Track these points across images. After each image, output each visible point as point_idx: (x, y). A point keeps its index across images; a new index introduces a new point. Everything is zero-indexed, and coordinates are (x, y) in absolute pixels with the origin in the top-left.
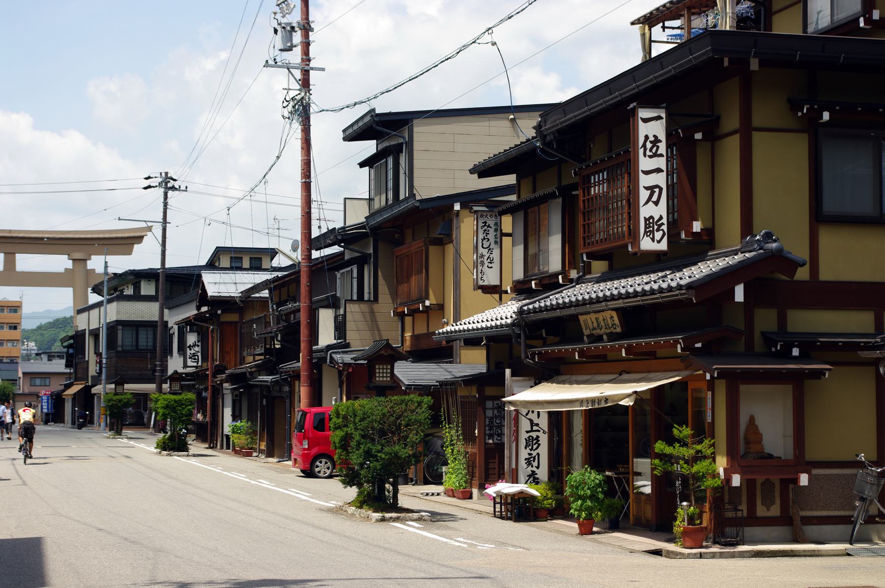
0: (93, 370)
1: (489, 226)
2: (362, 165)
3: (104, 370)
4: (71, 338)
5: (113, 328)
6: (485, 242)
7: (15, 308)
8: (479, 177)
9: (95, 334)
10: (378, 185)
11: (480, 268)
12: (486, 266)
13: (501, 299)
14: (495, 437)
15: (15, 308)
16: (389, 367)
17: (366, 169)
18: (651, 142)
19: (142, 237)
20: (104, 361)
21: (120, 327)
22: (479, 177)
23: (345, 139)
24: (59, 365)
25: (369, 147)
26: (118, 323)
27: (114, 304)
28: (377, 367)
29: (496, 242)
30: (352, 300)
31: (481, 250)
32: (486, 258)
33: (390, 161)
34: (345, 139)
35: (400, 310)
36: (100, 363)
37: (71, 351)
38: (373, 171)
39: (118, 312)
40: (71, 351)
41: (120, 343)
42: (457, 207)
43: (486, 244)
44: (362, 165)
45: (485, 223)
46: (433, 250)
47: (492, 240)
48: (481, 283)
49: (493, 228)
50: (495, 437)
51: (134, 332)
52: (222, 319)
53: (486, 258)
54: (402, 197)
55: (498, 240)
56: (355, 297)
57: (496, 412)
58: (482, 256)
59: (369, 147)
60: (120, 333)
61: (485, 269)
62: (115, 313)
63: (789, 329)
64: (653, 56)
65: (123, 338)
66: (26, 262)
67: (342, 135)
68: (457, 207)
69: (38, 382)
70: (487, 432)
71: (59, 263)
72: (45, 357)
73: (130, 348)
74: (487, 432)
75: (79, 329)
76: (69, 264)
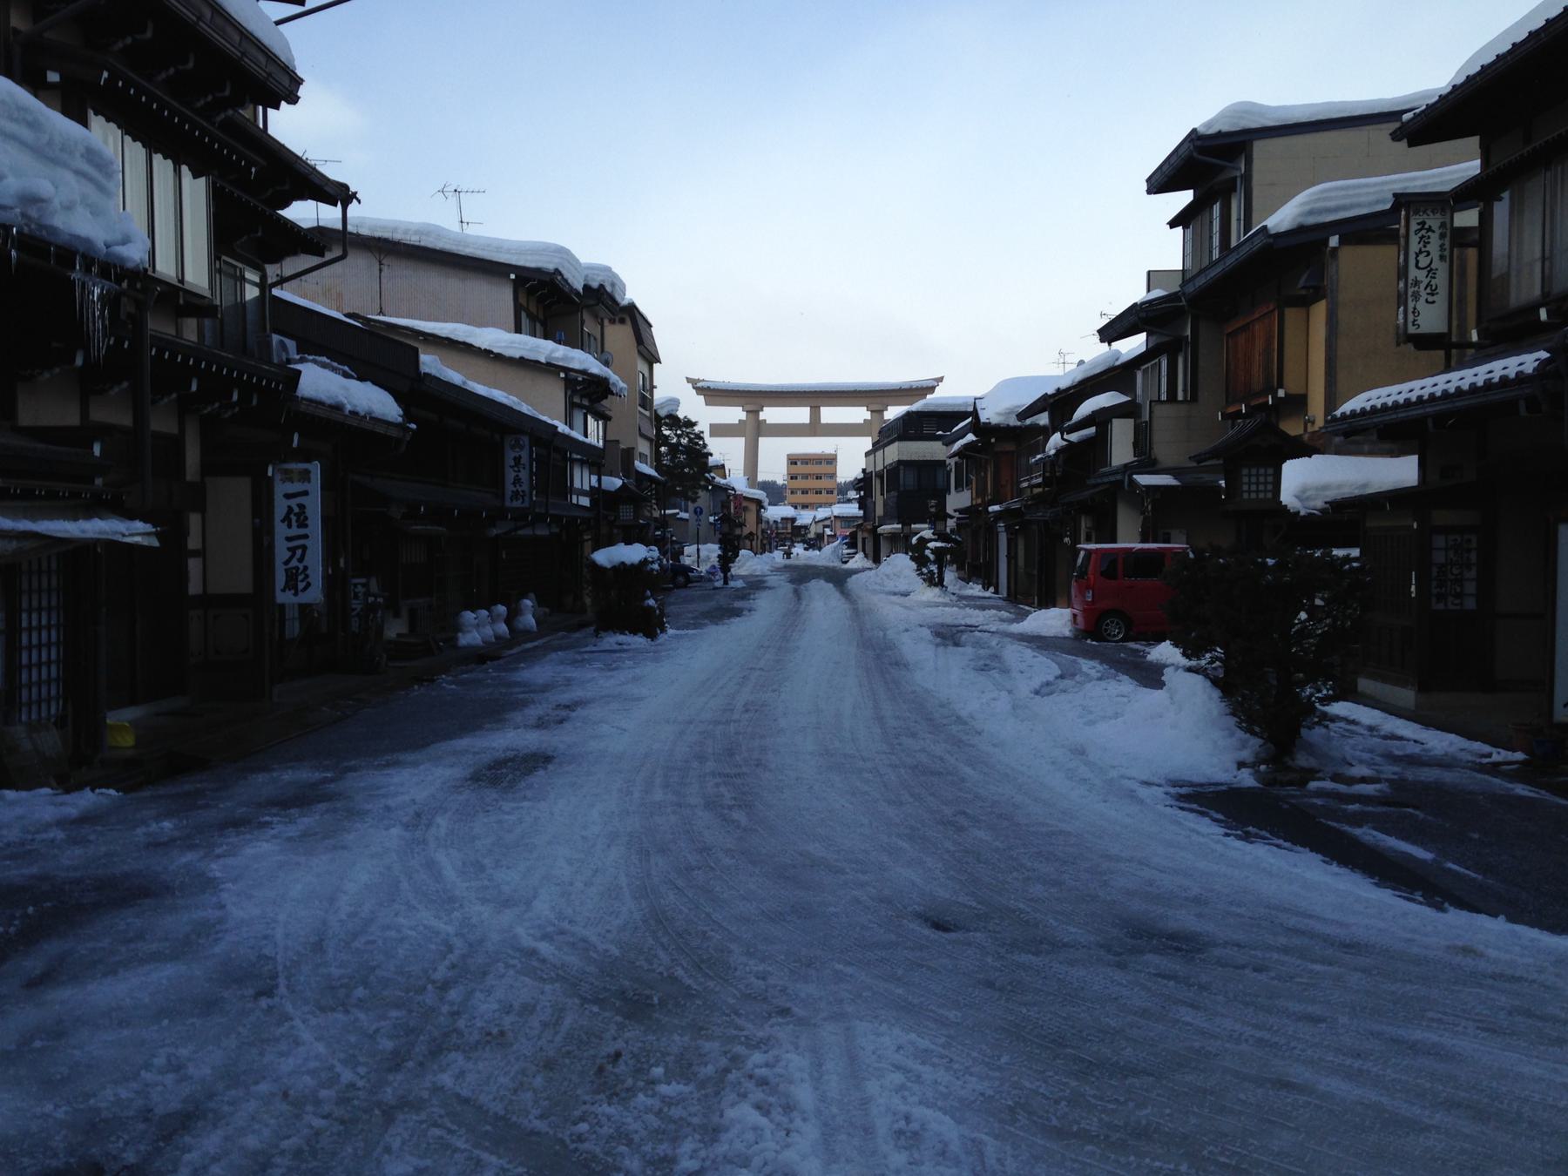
1: (1430, 229)
2: (1173, 224)
6: (1421, 257)
7: (831, 460)
8: (1410, 145)
10: (1194, 248)
11: (1411, 305)
12: (1422, 300)
13: (1448, 358)
14: (1450, 599)
15: (831, 460)
16: (1270, 471)
17: (1180, 229)
22: (1410, 145)
23: (1149, 192)
25: (1182, 199)
26: (900, 462)
28: (1245, 471)
29: (1442, 258)
30: (1159, 401)
31: (1413, 273)
32: (1422, 286)
33: (1217, 208)
34: (1149, 192)
35: (1231, 410)
38: (1189, 231)
42: (1334, 241)
43: (1424, 261)
44: (1173, 224)
45: (1423, 223)
46: (1292, 315)
47: (1435, 254)
48: (1412, 330)
49: (1438, 232)
50: (1450, 599)
52: (998, 449)
53: (1422, 286)
54: (1234, 243)
55: (1447, 253)
56: (1164, 397)
57: (1451, 554)
58: (1417, 283)
59: (1182, 199)
61: (1421, 305)
64: (1323, 302)
65: (908, 479)
66: (829, 415)
67: (1145, 187)
68: (1334, 241)
70: (1435, 591)
71: (858, 414)
74: (1435, 591)
76: (868, 415)
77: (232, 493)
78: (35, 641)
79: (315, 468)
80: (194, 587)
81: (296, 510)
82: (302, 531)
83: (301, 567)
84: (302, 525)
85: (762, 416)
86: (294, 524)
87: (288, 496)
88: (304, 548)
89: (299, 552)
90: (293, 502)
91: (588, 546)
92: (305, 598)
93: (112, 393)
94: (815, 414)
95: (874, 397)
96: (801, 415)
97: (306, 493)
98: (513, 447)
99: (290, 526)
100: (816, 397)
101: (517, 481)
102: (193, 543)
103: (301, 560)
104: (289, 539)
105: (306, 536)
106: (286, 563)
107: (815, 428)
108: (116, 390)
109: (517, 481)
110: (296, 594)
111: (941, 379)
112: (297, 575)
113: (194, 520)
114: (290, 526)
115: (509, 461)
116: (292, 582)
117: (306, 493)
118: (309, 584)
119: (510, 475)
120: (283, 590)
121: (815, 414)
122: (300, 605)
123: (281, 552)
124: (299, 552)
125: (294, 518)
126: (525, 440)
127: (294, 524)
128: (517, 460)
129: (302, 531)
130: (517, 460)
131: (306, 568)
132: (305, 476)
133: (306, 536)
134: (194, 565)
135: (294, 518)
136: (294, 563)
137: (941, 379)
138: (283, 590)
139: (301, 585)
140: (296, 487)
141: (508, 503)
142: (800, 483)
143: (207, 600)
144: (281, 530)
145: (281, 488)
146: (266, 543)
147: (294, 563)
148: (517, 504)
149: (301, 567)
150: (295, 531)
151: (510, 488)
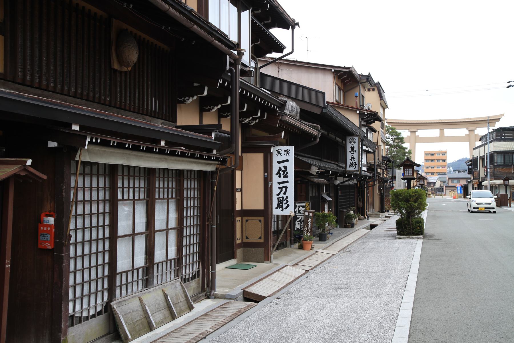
0: (482, 174)
3: (489, 174)
4: (471, 161)
5: (492, 156)
9: (483, 159)
18: (282, 171)
19: (499, 119)
20: (489, 170)
21: (496, 154)
24: (465, 175)
27: (493, 143)
36: (487, 171)
37: (470, 167)
39: (494, 147)
40: (470, 167)
41: (495, 161)
51: (503, 156)
60: (495, 157)
62: (493, 148)
63: (178, 105)
66: (449, 132)
69: (455, 181)
71: (463, 132)
72: (457, 172)
73: (500, 164)
75: (475, 157)
76: (467, 132)
77: (254, 161)
78: (87, 238)
79: (292, 148)
80: (238, 207)
81: (283, 169)
82: (285, 179)
83: (285, 197)
84: (286, 176)
85: (417, 134)
86: (282, 176)
87: (279, 162)
88: (286, 187)
89: (284, 189)
90: (282, 165)
91: (43, 214)
92: (286, 212)
93: (188, 102)
94: (442, 133)
95: (471, 124)
96: (435, 132)
97: (287, 161)
98: (350, 142)
99: (280, 177)
100: (442, 125)
101: (352, 158)
102: (238, 185)
103: (285, 194)
104: (279, 183)
105: (287, 182)
106: (278, 195)
107: (442, 139)
108: (191, 100)
109: (352, 158)
110: (282, 210)
111: (503, 115)
112: (283, 201)
113: (238, 173)
114: (280, 177)
115: (349, 149)
116: (280, 205)
117: (287, 161)
118: (288, 206)
119: (349, 155)
120: (277, 208)
121: (442, 133)
122: (283, 216)
123: (276, 190)
124: (284, 189)
125: (281, 173)
126: (356, 139)
127: (282, 176)
128: (353, 148)
129: (285, 179)
130: (353, 148)
131: (287, 198)
132: (287, 152)
133: (287, 182)
134: (238, 195)
135: (281, 173)
136: (282, 195)
137: (503, 115)
138: (277, 208)
139: (285, 206)
140: (283, 158)
141: (348, 169)
142: (430, 163)
143: (245, 213)
144: (276, 179)
145: (276, 158)
146: (270, 185)
147: (282, 195)
148: (352, 169)
149: (285, 197)
150: (282, 179)
151: (349, 162)
